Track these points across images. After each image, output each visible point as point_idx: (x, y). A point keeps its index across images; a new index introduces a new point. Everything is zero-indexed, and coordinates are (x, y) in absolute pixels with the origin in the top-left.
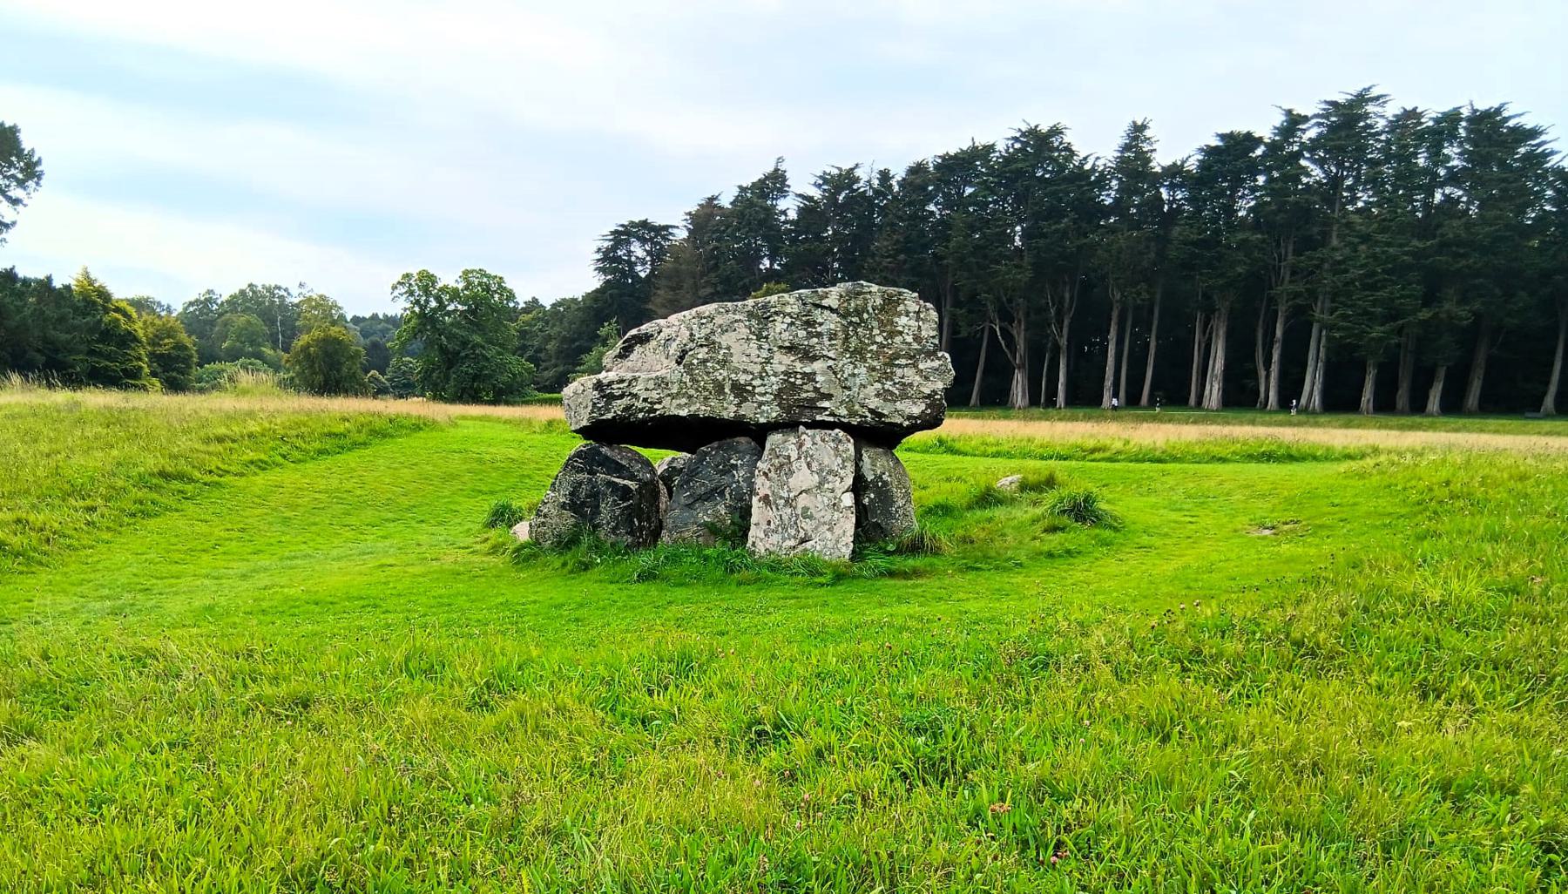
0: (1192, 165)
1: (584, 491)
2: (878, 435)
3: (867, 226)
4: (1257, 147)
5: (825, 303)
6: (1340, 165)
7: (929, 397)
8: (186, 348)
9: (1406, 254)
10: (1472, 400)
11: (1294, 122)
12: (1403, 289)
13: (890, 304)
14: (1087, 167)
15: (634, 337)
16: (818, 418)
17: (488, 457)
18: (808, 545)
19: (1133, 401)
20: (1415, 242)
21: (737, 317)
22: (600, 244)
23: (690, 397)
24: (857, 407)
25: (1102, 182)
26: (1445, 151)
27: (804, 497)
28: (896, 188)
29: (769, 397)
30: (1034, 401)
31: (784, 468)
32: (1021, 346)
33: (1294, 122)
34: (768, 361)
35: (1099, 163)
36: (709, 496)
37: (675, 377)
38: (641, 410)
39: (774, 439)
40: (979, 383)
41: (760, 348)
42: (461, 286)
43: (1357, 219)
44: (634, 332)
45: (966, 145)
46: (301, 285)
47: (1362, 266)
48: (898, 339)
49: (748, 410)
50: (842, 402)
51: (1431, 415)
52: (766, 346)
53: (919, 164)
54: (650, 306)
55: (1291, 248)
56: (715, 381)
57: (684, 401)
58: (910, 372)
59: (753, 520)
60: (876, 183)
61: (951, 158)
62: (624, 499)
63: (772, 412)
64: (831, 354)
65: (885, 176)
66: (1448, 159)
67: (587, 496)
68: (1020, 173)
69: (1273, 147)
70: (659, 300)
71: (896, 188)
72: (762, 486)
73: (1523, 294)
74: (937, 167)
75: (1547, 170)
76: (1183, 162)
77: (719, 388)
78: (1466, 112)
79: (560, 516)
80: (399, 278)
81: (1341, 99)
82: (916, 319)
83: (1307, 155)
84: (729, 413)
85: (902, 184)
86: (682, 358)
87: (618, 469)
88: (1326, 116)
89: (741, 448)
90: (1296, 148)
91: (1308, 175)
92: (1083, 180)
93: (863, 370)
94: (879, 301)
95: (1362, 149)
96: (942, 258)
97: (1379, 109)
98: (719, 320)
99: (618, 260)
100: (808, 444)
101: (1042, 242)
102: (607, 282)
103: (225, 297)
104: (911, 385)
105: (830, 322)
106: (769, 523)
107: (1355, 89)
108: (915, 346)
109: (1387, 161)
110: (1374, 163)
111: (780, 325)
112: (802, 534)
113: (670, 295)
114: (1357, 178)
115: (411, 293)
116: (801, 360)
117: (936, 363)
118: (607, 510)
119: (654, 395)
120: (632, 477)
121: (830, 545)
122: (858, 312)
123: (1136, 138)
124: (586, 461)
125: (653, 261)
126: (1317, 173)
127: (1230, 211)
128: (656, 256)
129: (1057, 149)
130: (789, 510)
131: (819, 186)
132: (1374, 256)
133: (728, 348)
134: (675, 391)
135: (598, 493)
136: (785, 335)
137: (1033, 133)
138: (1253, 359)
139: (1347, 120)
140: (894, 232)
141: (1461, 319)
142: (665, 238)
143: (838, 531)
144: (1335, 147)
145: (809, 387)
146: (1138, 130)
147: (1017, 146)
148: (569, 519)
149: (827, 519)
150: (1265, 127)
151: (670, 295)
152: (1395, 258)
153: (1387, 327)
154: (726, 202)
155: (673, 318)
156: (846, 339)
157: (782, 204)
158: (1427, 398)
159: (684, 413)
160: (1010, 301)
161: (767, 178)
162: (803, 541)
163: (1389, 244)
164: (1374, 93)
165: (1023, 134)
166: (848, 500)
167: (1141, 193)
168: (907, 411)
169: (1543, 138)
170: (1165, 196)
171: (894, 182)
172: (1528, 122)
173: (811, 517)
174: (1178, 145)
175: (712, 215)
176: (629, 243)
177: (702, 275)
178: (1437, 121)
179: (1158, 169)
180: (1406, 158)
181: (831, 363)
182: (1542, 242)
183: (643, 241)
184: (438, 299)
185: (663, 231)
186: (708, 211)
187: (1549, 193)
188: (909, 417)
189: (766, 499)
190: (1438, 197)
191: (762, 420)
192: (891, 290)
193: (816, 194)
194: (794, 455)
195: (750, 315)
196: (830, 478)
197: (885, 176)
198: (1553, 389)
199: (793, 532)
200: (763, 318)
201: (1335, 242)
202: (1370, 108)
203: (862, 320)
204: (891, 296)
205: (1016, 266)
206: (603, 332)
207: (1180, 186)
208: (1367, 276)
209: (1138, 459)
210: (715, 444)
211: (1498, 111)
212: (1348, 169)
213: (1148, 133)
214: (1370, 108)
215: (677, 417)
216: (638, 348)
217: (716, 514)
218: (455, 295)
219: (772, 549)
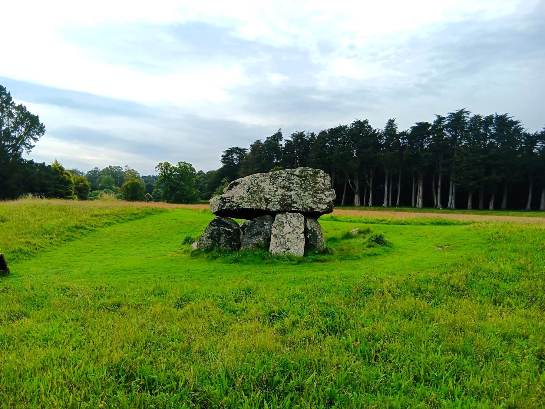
0: (409, 132)
1: (215, 233)
2: (312, 215)
5: (294, 173)
6: (456, 132)
7: (328, 203)
8: (87, 186)
11: (440, 119)
13: (315, 174)
14: (376, 132)
18: (289, 251)
19: (394, 205)
22: (223, 154)
23: (251, 202)
31: (281, 225)
32: (357, 187)
34: (276, 191)
36: (256, 234)
37: (247, 196)
38: (235, 206)
39: (278, 216)
40: (344, 198)
41: (274, 187)
42: (178, 167)
44: (233, 182)
45: (338, 126)
46: (126, 166)
48: (318, 185)
49: (270, 207)
51: (490, 210)
54: (238, 173)
57: (249, 203)
58: (322, 195)
59: (271, 242)
60: (310, 137)
63: (278, 207)
66: (490, 130)
67: (217, 234)
69: (434, 127)
76: (406, 131)
77: (260, 200)
78: (494, 116)
79: (207, 241)
80: (158, 164)
81: (455, 112)
82: (324, 179)
84: (263, 207)
85: (318, 137)
86: (249, 190)
88: (451, 117)
89: (268, 219)
91: (446, 135)
92: (374, 136)
93: (307, 194)
94: (312, 173)
98: (260, 178)
99: (229, 159)
100: (289, 217)
102: (225, 166)
103: (101, 169)
104: (322, 199)
105: (296, 179)
107: (459, 109)
108: (323, 187)
109: (471, 131)
111: (280, 180)
112: (287, 247)
114: (462, 136)
115: (162, 169)
116: (287, 191)
117: (330, 193)
119: (239, 202)
120: (232, 228)
121: (296, 251)
122: (305, 176)
123: (391, 124)
124: (217, 222)
125: (239, 160)
126: (449, 135)
128: (240, 158)
129: (366, 127)
136: (282, 183)
137: (359, 122)
138: (432, 192)
146: (391, 122)
148: (210, 242)
149: (295, 242)
150: (431, 120)
154: (263, 142)
155: (246, 178)
156: (301, 185)
157: (281, 143)
159: (249, 207)
162: (288, 250)
164: (466, 110)
165: (356, 123)
166: (302, 236)
167: (393, 140)
169: (519, 124)
172: (514, 119)
174: (404, 126)
175: (258, 146)
176: (232, 154)
178: (486, 119)
181: (296, 192)
183: (236, 153)
184: (170, 171)
188: (322, 209)
189: (275, 236)
191: (274, 210)
192: (316, 170)
193: (291, 139)
194: (285, 221)
195: (271, 177)
196: (297, 229)
197: (313, 134)
198: (529, 202)
199: (284, 246)
200: (274, 178)
201: (456, 156)
202: (465, 115)
204: (315, 171)
206: (223, 181)
210: (259, 218)
211: (505, 116)
213: (395, 123)
214: (465, 115)
218: (176, 169)
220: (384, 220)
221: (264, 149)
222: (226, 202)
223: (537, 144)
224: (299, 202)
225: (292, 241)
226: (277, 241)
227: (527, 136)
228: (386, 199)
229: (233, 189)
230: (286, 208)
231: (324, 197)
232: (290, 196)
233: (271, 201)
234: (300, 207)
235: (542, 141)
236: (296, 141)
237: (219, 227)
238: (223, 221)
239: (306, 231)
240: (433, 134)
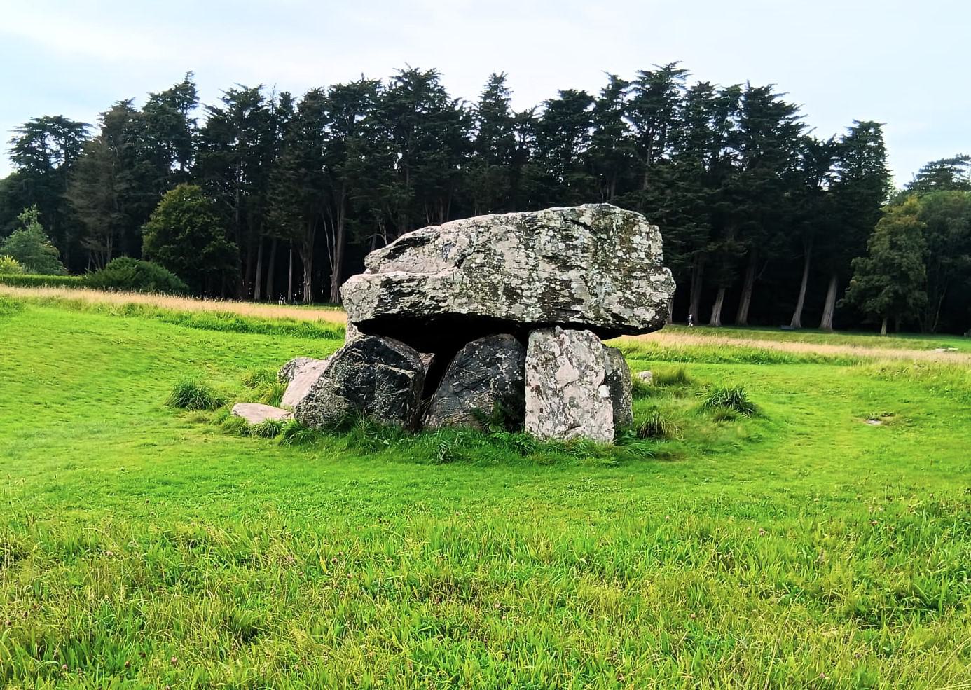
0: (539, 114)
3: (269, 138)
4: (590, 104)
5: (582, 220)
6: (651, 124)
7: (657, 305)
9: (699, 198)
10: (743, 315)
11: (617, 86)
12: (697, 226)
13: (629, 223)
14: (457, 108)
15: (408, 240)
16: (571, 319)
17: (112, 339)
18: (578, 430)
20: (706, 190)
21: (510, 228)
22: (15, 135)
23: (469, 297)
24: (602, 311)
25: (468, 122)
26: (729, 119)
28: (296, 110)
29: (534, 300)
31: (549, 362)
33: (617, 86)
34: (534, 268)
35: (466, 106)
36: (475, 386)
37: (458, 278)
38: (427, 307)
39: (536, 337)
41: (528, 256)
43: (663, 168)
44: (409, 235)
45: (356, 79)
47: (668, 207)
48: (634, 255)
49: (517, 310)
50: (590, 307)
51: (714, 326)
52: (533, 255)
53: (316, 91)
54: (65, 196)
55: (613, 188)
56: (491, 284)
57: (464, 300)
58: (643, 283)
59: (528, 407)
60: (278, 104)
61: (344, 89)
62: (400, 386)
63: (536, 313)
64: (583, 265)
65: (286, 98)
66: (731, 125)
67: (363, 383)
68: (402, 108)
69: (602, 106)
70: (76, 191)
71: (296, 110)
72: (533, 378)
73: (780, 234)
74: (332, 95)
75: (799, 139)
76: (533, 110)
77: (494, 289)
78: (744, 89)
79: (333, 401)
81: (653, 70)
82: (647, 240)
83: (626, 114)
84: (501, 312)
85: (302, 107)
86: (461, 261)
88: (643, 83)
89: (506, 343)
90: (618, 108)
91: (627, 130)
92: (453, 118)
93: (609, 280)
94: (621, 222)
95: (668, 111)
96: (339, 174)
97: (681, 81)
98: (494, 230)
99: (33, 151)
100: (567, 342)
101: (422, 168)
102: (22, 171)
104: (644, 294)
106: (541, 411)
107: (664, 63)
108: (647, 261)
109: (686, 123)
110: (676, 125)
111: (544, 237)
112: (571, 421)
113: (87, 187)
114: (662, 136)
116: (560, 268)
117: (663, 277)
118: (380, 397)
119: (440, 294)
120: (409, 367)
121: (595, 430)
122: (607, 230)
123: (496, 88)
124: (365, 351)
126: (634, 129)
127: (567, 153)
128: (71, 149)
129: (432, 90)
130: (557, 400)
131: (227, 101)
132: (676, 198)
133: (502, 255)
134: (457, 291)
135: (375, 380)
136: (549, 246)
137: (413, 75)
139: (657, 86)
140: (295, 147)
141: (738, 251)
142: (78, 134)
143: (599, 418)
144: (649, 109)
146: (497, 80)
147: (400, 84)
148: (343, 403)
149: (589, 408)
150: (595, 88)
151: (87, 187)
152: (691, 201)
153: (685, 255)
154: (139, 106)
155: (448, 225)
157: (191, 114)
158: (711, 312)
159: (464, 311)
160: (395, 216)
161: (177, 89)
162: (572, 427)
163: (687, 190)
164: (678, 68)
165: (405, 75)
167: (497, 132)
168: (642, 317)
169: (796, 114)
170: (517, 138)
171: (294, 104)
173: (577, 406)
174: (529, 97)
176: (42, 136)
177: (118, 171)
178: (723, 94)
179: (513, 116)
180: (700, 123)
181: (583, 272)
182: (793, 194)
183: (57, 135)
185: (75, 128)
186: (123, 113)
187: (800, 156)
188: (644, 322)
189: (537, 390)
190: (722, 153)
191: (528, 320)
192: (629, 212)
193: (225, 108)
194: (557, 352)
195: (519, 227)
196: (588, 372)
197: (286, 98)
198: (799, 308)
199: (563, 419)
200: (530, 229)
201: (646, 185)
202: (675, 80)
203: (609, 237)
204: (629, 217)
205: (402, 187)
206: (23, 216)
207: (529, 131)
208: (675, 213)
209: (803, 361)
210: (483, 340)
211: (767, 90)
212: (657, 128)
213: (505, 85)
215: (459, 314)
217: (481, 402)
219: (547, 433)
220: (635, 350)
221: (143, 129)
223: (832, 167)
225: (582, 405)
226: (543, 402)
227: (811, 145)
230: (557, 317)
231: (649, 290)
233: (521, 296)
234: (591, 315)
235: (842, 160)
236: (240, 111)
237: (371, 362)
240: (596, 124)
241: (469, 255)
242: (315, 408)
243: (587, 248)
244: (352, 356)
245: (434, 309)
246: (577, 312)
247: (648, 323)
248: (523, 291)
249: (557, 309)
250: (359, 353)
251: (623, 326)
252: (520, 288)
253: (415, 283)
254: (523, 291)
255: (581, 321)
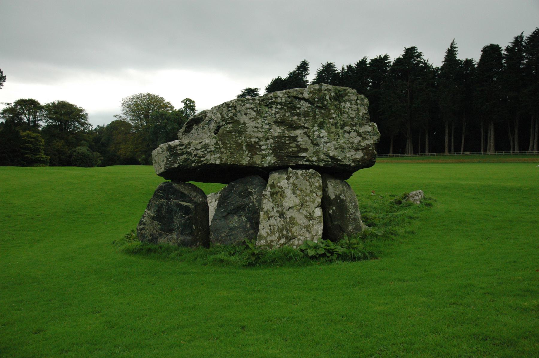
1: (164, 209)
2: (336, 171)
16: (300, 163)
19: (457, 150)
27: (292, 208)
30: (416, 151)
38: (193, 162)
39: (274, 177)
40: (390, 145)
49: (257, 160)
63: (271, 160)
64: (306, 125)
72: (267, 205)
77: (239, 146)
79: (152, 224)
84: (245, 161)
87: (183, 197)
92: (322, 70)
118: (177, 220)
119: (200, 153)
120: (191, 201)
124: (164, 192)
145: (293, 145)
166: (318, 212)
181: (306, 130)
188: (354, 161)
191: (265, 165)
192: (340, 88)
216: (195, 127)
222: (177, 155)
224: (311, 149)
228: (446, 144)
229: (193, 131)
232: (294, 139)
237: (168, 199)
238: (176, 190)
239: (325, 204)
241: (223, 125)
242: (143, 229)
243: (308, 114)
244: (158, 196)
245: (198, 162)
246: (304, 157)
247: (358, 161)
248: (261, 146)
249: (287, 156)
250: (162, 193)
251: (339, 164)
252: (258, 145)
253: (184, 147)
254: (261, 146)
255: (307, 163)
